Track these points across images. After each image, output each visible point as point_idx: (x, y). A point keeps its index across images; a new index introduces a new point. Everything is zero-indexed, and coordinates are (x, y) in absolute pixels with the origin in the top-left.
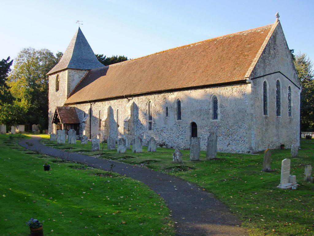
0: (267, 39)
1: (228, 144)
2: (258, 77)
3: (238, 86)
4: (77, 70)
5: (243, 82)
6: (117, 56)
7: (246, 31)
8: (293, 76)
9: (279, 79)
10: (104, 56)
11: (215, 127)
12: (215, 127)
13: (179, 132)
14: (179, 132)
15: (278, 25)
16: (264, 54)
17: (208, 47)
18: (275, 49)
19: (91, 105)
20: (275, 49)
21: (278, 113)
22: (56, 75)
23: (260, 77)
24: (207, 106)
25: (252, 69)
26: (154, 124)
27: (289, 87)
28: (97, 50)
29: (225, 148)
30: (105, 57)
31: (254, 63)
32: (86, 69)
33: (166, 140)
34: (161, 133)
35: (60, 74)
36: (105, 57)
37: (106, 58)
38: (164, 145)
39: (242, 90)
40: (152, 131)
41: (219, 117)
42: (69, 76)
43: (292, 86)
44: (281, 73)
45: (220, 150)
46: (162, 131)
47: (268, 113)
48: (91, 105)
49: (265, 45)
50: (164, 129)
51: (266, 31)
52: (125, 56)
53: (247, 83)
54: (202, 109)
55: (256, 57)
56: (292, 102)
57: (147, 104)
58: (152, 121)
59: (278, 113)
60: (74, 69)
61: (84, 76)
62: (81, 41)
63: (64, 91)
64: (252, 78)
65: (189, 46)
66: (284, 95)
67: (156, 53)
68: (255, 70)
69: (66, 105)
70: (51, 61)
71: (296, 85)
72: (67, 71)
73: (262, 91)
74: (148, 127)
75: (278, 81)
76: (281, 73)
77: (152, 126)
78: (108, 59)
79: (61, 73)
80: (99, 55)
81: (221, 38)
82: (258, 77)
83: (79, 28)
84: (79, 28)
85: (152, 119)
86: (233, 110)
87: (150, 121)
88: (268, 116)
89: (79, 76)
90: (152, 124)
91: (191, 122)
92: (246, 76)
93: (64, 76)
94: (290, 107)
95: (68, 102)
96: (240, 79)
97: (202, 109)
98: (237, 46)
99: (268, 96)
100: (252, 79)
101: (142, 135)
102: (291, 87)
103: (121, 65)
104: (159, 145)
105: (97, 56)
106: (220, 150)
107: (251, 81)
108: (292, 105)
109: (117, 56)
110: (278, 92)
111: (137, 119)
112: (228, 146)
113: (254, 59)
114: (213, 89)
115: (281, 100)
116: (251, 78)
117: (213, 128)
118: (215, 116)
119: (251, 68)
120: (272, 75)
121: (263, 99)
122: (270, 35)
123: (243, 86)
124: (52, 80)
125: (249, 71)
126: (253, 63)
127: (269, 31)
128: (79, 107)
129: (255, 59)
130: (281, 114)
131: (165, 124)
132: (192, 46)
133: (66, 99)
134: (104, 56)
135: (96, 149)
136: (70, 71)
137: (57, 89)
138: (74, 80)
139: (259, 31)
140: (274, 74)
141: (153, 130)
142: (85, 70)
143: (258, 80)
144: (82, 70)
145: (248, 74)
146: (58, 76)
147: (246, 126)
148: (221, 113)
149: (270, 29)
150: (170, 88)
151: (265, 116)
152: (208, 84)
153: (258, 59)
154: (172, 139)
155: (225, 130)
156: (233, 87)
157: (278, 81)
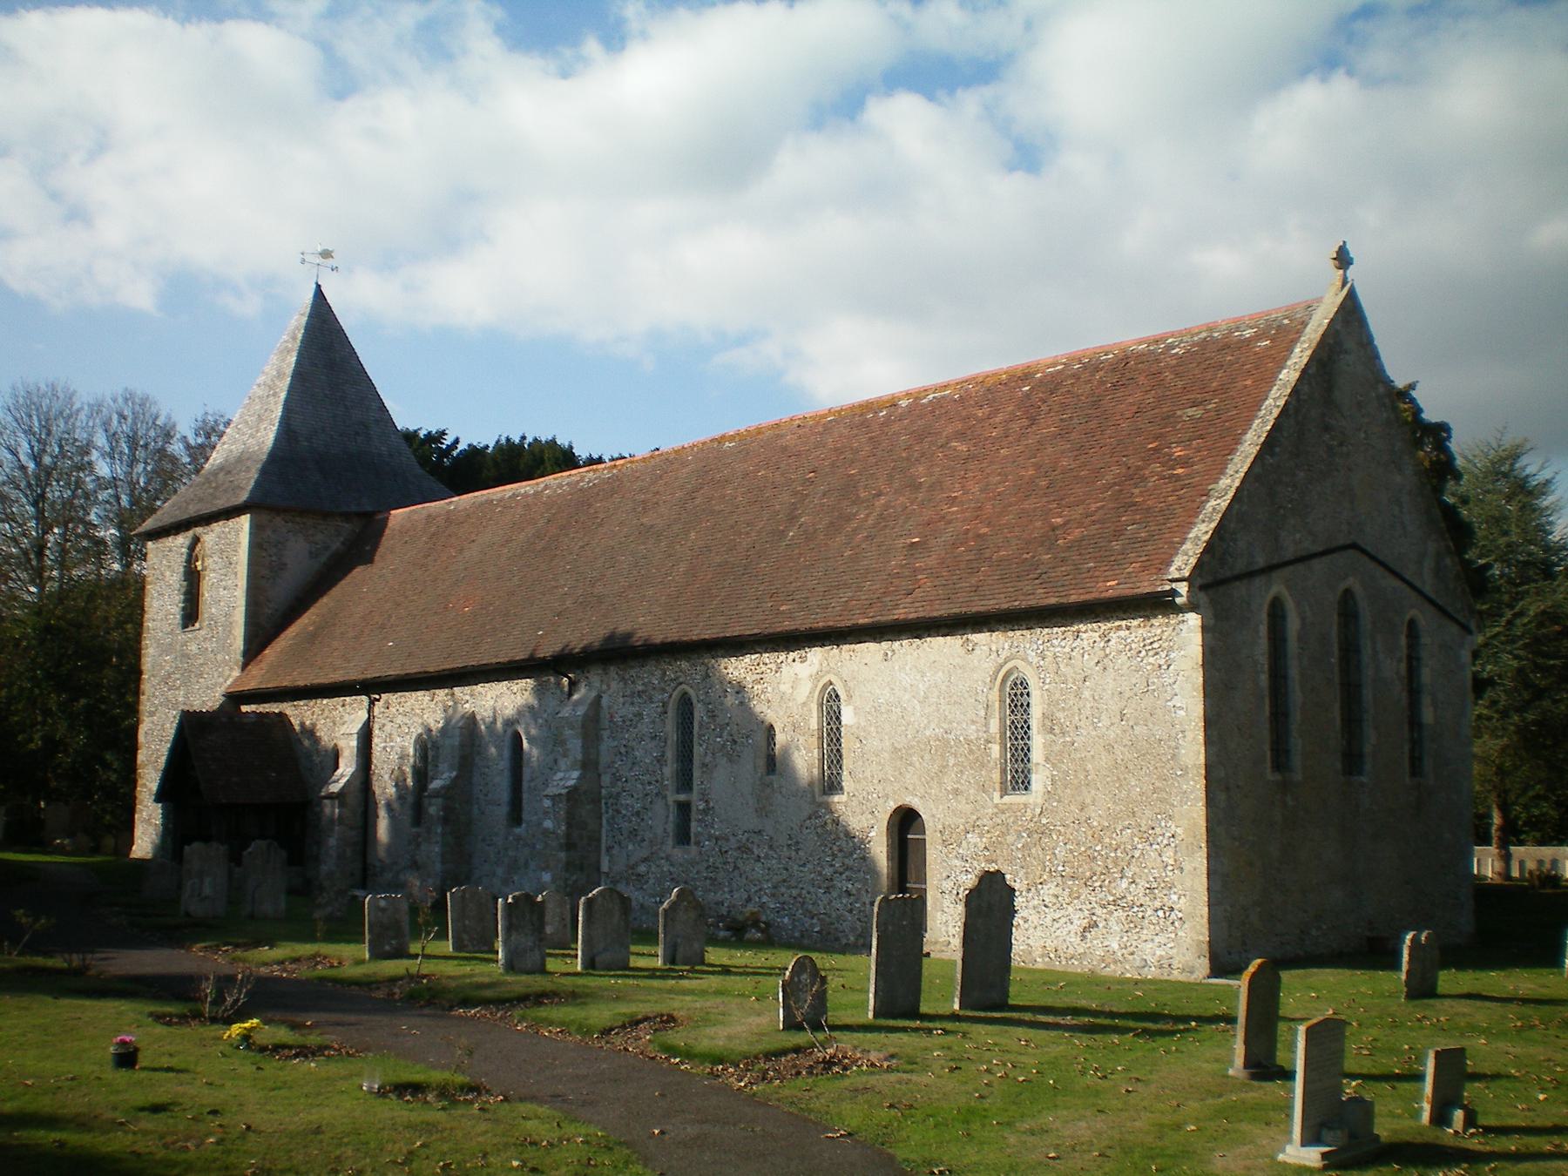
0: (1289, 376)
1: (1085, 923)
2: (1238, 578)
3: (1135, 623)
4: (303, 512)
5: (1157, 604)
6: (524, 438)
7: (1181, 334)
8: (1429, 563)
9: (1352, 582)
10: (448, 440)
11: (1020, 836)
12: (1020, 836)
13: (834, 856)
14: (834, 856)
15: (1342, 307)
16: (1272, 455)
17: (987, 410)
18: (1327, 428)
19: (372, 703)
20: (1327, 428)
21: (1352, 760)
22: (181, 541)
23: (1250, 575)
24: (973, 722)
25: (1207, 537)
26: (705, 812)
27: (1412, 624)
28: (410, 410)
29: (1075, 944)
30: (457, 441)
31: (1217, 505)
32: (354, 508)
33: (765, 899)
34: (740, 864)
35: (211, 536)
36: (457, 441)
37: (462, 446)
38: (756, 924)
39: (1156, 645)
40: (693, 849)
41: (1038, 780)
42: (256, 546)
43: (1425, 618)
44: (1364, 551)
45: (1042, 956)
46: (744, 849)
47: (1297, 761)
48: (372, 703)
49: (1276, 412)
50: (756, 839)
51: (1283, 333)
52: (562, 441)
53: (1180, 610)
54: (952, 736)
55: (1230, 471)
56: (1426, 700)
57: (665, 705)
58: (694, 797)
59: (1352, 760)
60: (285, 511)
61: (336, 545)
62: (326, 351)
63: (229, 627)
64: (1209, 579)
65: (892, 403)
66: (1382, 665)
67: (723, 437)
68: (1221, 539)
69: (235, 698)
70: (166, 486)
71: (1450, 609)
72: (245, 521)
73: (1263, 644)
74: (670, 827)
75: (1348, 593)
76: (1364, 551)
77: (693, 824)
78: (475, 453)
79: (217, 527)
80: (422, 434)
81: (1054, 365)
82: (1238, 578)
83: (318, 286)
84: (319, 294)
85: (691, 789)
86: (1109, 748)
87: (682, 797)
88: (1298, 776)
89: (299, 553)
90: (694, 815)
91: (892, 805)
92: (1173, 573)
93: (230, 549)
94: (1415, 723)
95: (251, 685)
96: (1145, 588)
97: (952, 736)
98: (1134, 409)
99: (1294, 672)
100: (1203, 588)
101: (642, 869)
102: (1422, 622)
103: (536, 494)
104: (728, 928)
105: (410, 437)
106: (1042, 956)
107: (1203, 598)
108: (1428, 716)
109: (524, 438)
110: (1349, 650)
111: (613, 784)
112: (1084, 938)
113: (1216, 481)
114: (1010, 634)
115: (1368, 694)
116: (1199, 581)
117: (1010, 839)
118: (1019, 780)
119: (1202, 531)
120: (1315, 563)
121: (1266, 693)
122: (1300, 355)
123: (1158, 621)
124: (162, 565)
125: (1188, 546)
126: (1213, 502)
127: (1300, 332)
128: (299, 713)
129: (1224, 482)
130: (1368, 767)
131: (762, 811)
132: (904, 403)
133: (236, 673)
134: (448, 440)
135: (387, 948)
136: (265, 517)
137: (191, 614)
138: (282, 566)
139: (1248, 333)
140: (1325, 559)
141: (697, 843)
142: (347, 516)
143: (1239, 590)
144: (326, 515)
145: (1184, 562)
146: (196, 540)
147: (1179, 831)
148: (1047, 760)
149: (1304, 324)
150: (788, 625)
151: (1278, 777)
152: (982, 609)
153: (1237, 483)
154: (795, 892)
155: (1071, 851)
156: (1105, 626)
157: (1348, 593)
